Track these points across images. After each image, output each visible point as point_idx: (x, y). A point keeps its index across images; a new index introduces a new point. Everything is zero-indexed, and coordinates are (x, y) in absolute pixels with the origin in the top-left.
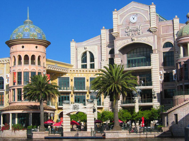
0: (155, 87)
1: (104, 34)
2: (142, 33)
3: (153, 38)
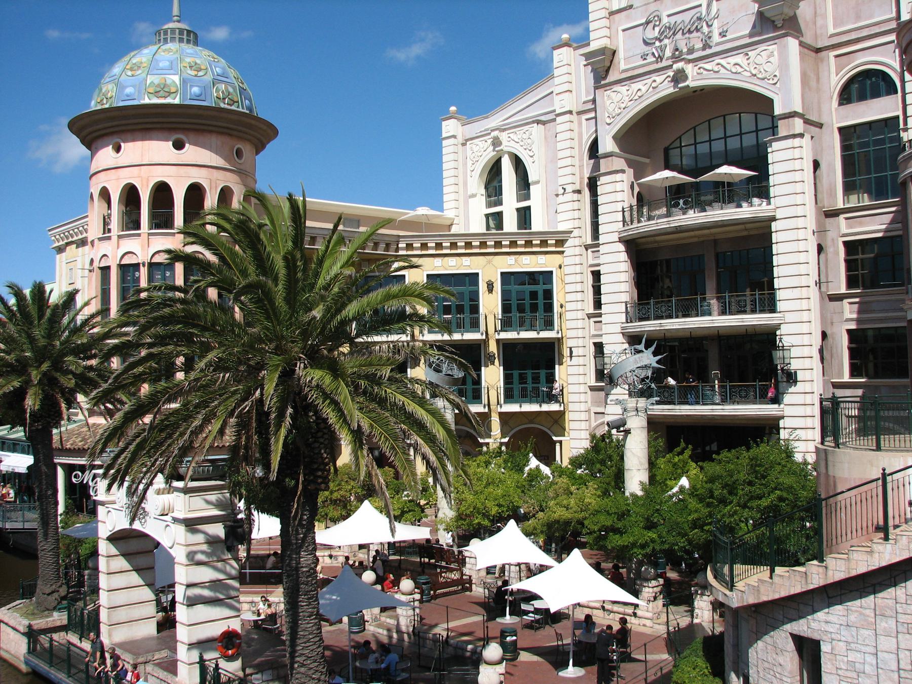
0: (789, 317)
1: (565, 70)
2: (723, 34)
3: (776, 53)
